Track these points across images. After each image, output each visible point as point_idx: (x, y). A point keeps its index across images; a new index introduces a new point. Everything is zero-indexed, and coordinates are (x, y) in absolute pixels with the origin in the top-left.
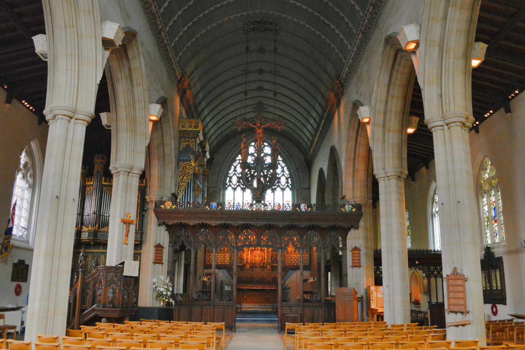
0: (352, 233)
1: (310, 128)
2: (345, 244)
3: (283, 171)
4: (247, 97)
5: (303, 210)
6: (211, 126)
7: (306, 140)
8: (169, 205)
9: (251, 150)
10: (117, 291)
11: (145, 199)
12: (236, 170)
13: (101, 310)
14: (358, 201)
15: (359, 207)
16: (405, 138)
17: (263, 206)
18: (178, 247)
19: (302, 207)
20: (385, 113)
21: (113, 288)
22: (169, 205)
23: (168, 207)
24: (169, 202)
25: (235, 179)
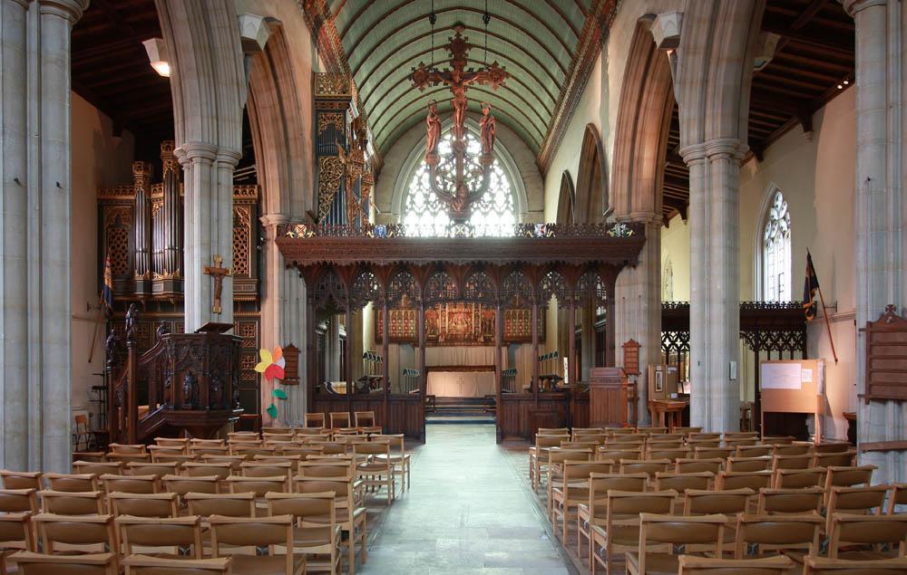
0: (624, 276)
1: (546, 100)
2: (611, 295)
3: (500, 183)
4: (436, 26)
5: (540, 234)
6: (376, 101)
7: (539, 124)
8: (301, 231)
9: (445, 148)
10: (200, 378)
11: (259, 223)
12: (419, 183)
13: (171, 414)
14: (636, 216)
15: (638, 228)
16: (748, 77)
17: (467, 229)
18: (322, 305)
19: (536, 229)
20: (713, 22)
21: (191, 374)
22: (301, 231)
23: (301, 235)
24: (301, 226)
25: (419, 199)
